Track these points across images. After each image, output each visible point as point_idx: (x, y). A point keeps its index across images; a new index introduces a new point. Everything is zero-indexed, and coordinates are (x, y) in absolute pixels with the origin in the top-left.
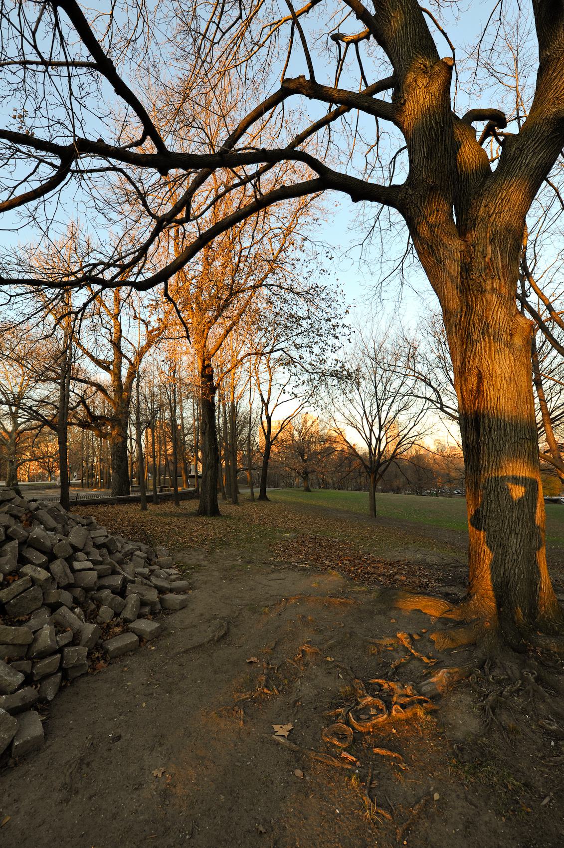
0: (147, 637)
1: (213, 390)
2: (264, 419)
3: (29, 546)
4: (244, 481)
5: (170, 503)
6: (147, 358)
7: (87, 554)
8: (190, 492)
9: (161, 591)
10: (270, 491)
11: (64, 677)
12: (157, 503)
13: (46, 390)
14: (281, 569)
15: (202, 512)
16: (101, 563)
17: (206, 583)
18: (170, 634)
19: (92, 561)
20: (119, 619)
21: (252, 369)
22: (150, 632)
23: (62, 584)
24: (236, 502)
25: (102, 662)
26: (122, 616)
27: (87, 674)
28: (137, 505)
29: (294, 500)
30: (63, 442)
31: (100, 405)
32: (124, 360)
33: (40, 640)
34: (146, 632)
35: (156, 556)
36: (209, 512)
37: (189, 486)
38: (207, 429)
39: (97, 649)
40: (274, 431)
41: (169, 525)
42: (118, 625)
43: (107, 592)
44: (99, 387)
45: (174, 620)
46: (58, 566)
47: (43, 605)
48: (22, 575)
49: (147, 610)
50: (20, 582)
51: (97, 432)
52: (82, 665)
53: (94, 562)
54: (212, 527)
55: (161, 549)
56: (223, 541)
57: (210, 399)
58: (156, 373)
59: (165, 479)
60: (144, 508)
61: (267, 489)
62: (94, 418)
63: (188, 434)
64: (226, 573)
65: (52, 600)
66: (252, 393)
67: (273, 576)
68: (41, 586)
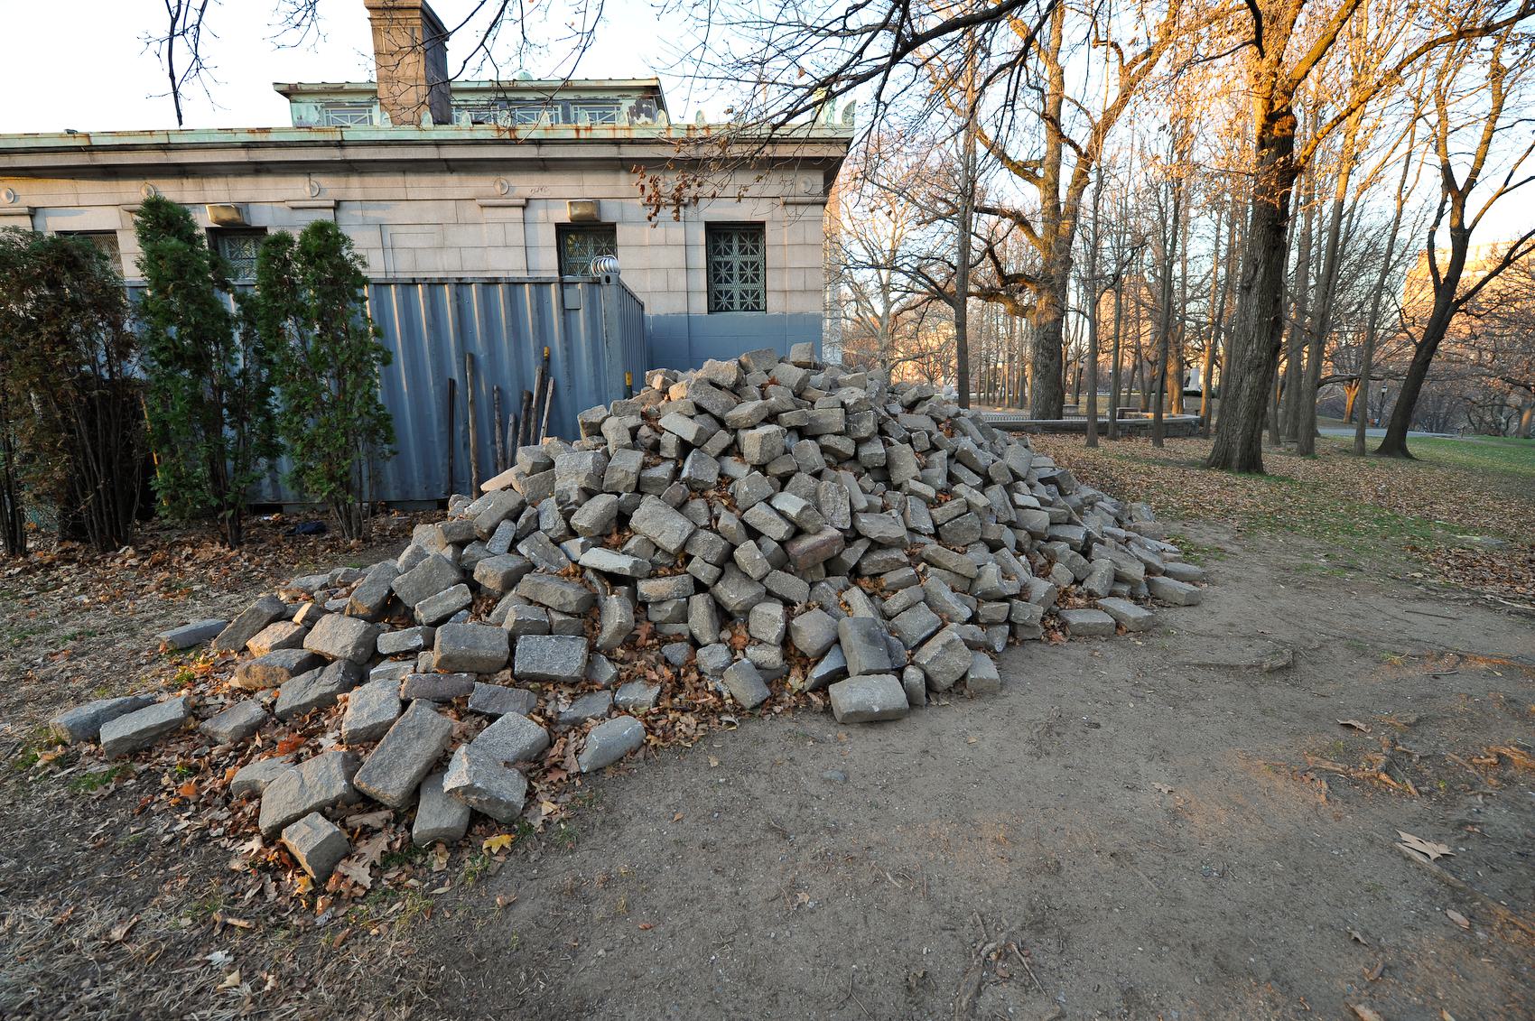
0: (1126, 626)
1: (1290, 173)
2: (1444, 241)
3: (958, 461)
4: (1335, 410)
5: (1141, 439)
6: (1120, 130)
7: (1031, 486)
8: (1187, 423)
9: (1150, 570)
10: (1416, 439)
11: (1012, 634)
12: (1115, 438)
13: (938, 239)
14: (1448, 599)
15: (1220, 461)
16: (1050, 504)
17: (1238, 580)
18: (1167, 634)
19: (1038, 498)
20: (1080, 588)
21: (1427, 91)
22: (1135, 620)
23: (1003, 520)
24: (1307, 451)
25: (1060, 634)
26: (1085, 585)
27: (1040, 640)
28: (1076, 438)
29: (1504, 466)
30: (961, 325)
31: (1020, 253)
32: (1068, 151)
33: (985, 578)
34: (1128, 617)
35: (1130, 518)
36: (1235, 463)
37: (1183, 412)
38: (1259, 277)
39: (1051, 615)
40: (1470, 275)
41: (1148, 475)
42: (1079, 596)
43: (1064, 546)
44: (1020, 220)
45: (1177, 618)
46: (996, 492)
47: (981, 539)
48: (955, 496)
49: (1125, 589)
50: (954, 503)
51: (1009, 306)
52: (1035, 627)
53: (1043, 502)
54: (1246, 492)
55: (1143, 513)
56: (1277, 520)
57: (1276, 202)
58: (1137, 163)
59: (1129, 396)
60: (1093, 444)
61: (1409, 434)
62: (1006, 279)
63: (1192, 298)
64: (1286, 575)
65: (992, 536)
66: (1413, 167)
67: (1418, 606)
68: (978, 514)
